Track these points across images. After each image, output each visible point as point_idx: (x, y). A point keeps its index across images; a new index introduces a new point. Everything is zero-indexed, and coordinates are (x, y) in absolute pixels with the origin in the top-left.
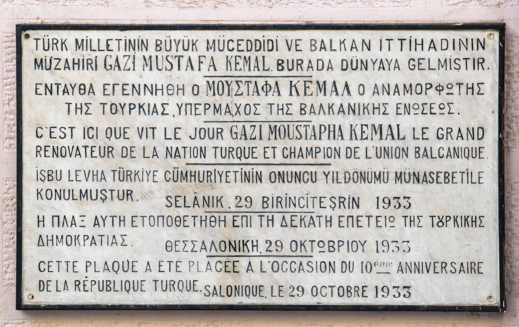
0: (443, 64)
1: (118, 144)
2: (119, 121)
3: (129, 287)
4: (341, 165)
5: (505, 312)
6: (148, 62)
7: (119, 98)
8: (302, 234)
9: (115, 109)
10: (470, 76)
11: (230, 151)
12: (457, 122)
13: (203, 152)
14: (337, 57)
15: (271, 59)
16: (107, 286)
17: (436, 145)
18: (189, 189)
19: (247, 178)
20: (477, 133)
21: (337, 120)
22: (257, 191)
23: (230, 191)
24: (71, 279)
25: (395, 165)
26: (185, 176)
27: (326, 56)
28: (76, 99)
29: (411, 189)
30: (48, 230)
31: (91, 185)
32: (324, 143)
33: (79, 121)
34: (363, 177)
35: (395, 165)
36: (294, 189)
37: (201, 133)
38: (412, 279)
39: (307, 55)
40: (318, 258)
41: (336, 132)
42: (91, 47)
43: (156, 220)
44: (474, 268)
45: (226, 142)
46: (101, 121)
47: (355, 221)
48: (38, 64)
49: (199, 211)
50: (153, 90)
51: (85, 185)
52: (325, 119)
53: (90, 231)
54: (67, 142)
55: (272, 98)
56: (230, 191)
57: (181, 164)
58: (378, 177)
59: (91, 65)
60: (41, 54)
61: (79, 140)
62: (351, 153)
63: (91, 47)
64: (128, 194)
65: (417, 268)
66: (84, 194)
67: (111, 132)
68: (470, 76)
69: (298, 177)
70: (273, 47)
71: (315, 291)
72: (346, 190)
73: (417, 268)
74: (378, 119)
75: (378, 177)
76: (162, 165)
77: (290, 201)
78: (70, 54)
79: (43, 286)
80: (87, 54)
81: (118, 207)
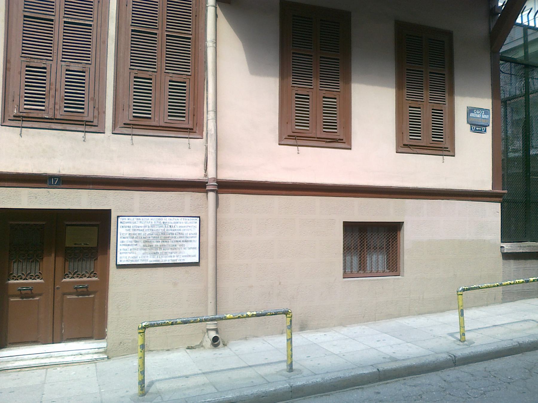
0: (190, 223)
1: (135, 236)
2: (135, 232)
3: (136, 261)
4: (173, 239)
5: (290, 311)
6: (140, 222)
7: (135, 228)
8: (167, 251)
9: (134, 230)
10: (194, 225)
11: (154, 237)
12: (193, 232)
13: (150, 237)
14: (173, 222)
15: (162, 222)
16: (132, 261)
17: (189, 236)
18: (147, 244)
19: (157, 242)
20: (196, 234)
21: (173, 232)
22: (159, 244)
23: (155, 244)
24: (126, 260)
25: (182, 239)
26: (146, 242)
27: (171, 221)
28: (128, 228)
29: (184, 243)
30: (122, 251)
31: (130, 243)
32: (171, 236)
33: (128, 232)
34: (177, 241)
35: (182, 239)
36: (165, 244)
37: (149, 234)
38: (184, 258)
39: (168, 221)
40: (169, 255)
41: (173, 234)
42: (69, 225)
43: (141, 249)
44: (194, 256)
45: (154, 236)
46: (132, 232)
47: (176, 249)
48: (121, 223)
49: (149, 248)
50: (141, 227)
51: (129, 243)
52: (171, 232)
53: (130, 251)
54: (126, 236)
55: (162, 228)
56: (155, 244)
57: (146, 239)
58: (180, 241)
59: (130, 223)
60: (122, 221)
61: (128, 236)
62: (175, 237)
63: (69, 225)
64: (136, 245)
65: (185, 256)
66: (128, 245)
67: (134, 234)
68: (194, 225)
69: (166, 242)
70: (162, 219)
71: (169, 261)
72: (174, 244)
73: (185, 256)
74: (180, 232)
75: (180, 241)
76: (143, 240)
77: (165, 246)
78: (127, 221)
79: (121, 261)
80: (129, 221)
81: (135, 247)
